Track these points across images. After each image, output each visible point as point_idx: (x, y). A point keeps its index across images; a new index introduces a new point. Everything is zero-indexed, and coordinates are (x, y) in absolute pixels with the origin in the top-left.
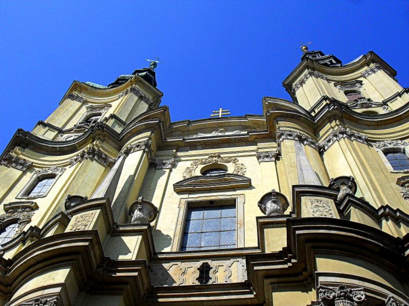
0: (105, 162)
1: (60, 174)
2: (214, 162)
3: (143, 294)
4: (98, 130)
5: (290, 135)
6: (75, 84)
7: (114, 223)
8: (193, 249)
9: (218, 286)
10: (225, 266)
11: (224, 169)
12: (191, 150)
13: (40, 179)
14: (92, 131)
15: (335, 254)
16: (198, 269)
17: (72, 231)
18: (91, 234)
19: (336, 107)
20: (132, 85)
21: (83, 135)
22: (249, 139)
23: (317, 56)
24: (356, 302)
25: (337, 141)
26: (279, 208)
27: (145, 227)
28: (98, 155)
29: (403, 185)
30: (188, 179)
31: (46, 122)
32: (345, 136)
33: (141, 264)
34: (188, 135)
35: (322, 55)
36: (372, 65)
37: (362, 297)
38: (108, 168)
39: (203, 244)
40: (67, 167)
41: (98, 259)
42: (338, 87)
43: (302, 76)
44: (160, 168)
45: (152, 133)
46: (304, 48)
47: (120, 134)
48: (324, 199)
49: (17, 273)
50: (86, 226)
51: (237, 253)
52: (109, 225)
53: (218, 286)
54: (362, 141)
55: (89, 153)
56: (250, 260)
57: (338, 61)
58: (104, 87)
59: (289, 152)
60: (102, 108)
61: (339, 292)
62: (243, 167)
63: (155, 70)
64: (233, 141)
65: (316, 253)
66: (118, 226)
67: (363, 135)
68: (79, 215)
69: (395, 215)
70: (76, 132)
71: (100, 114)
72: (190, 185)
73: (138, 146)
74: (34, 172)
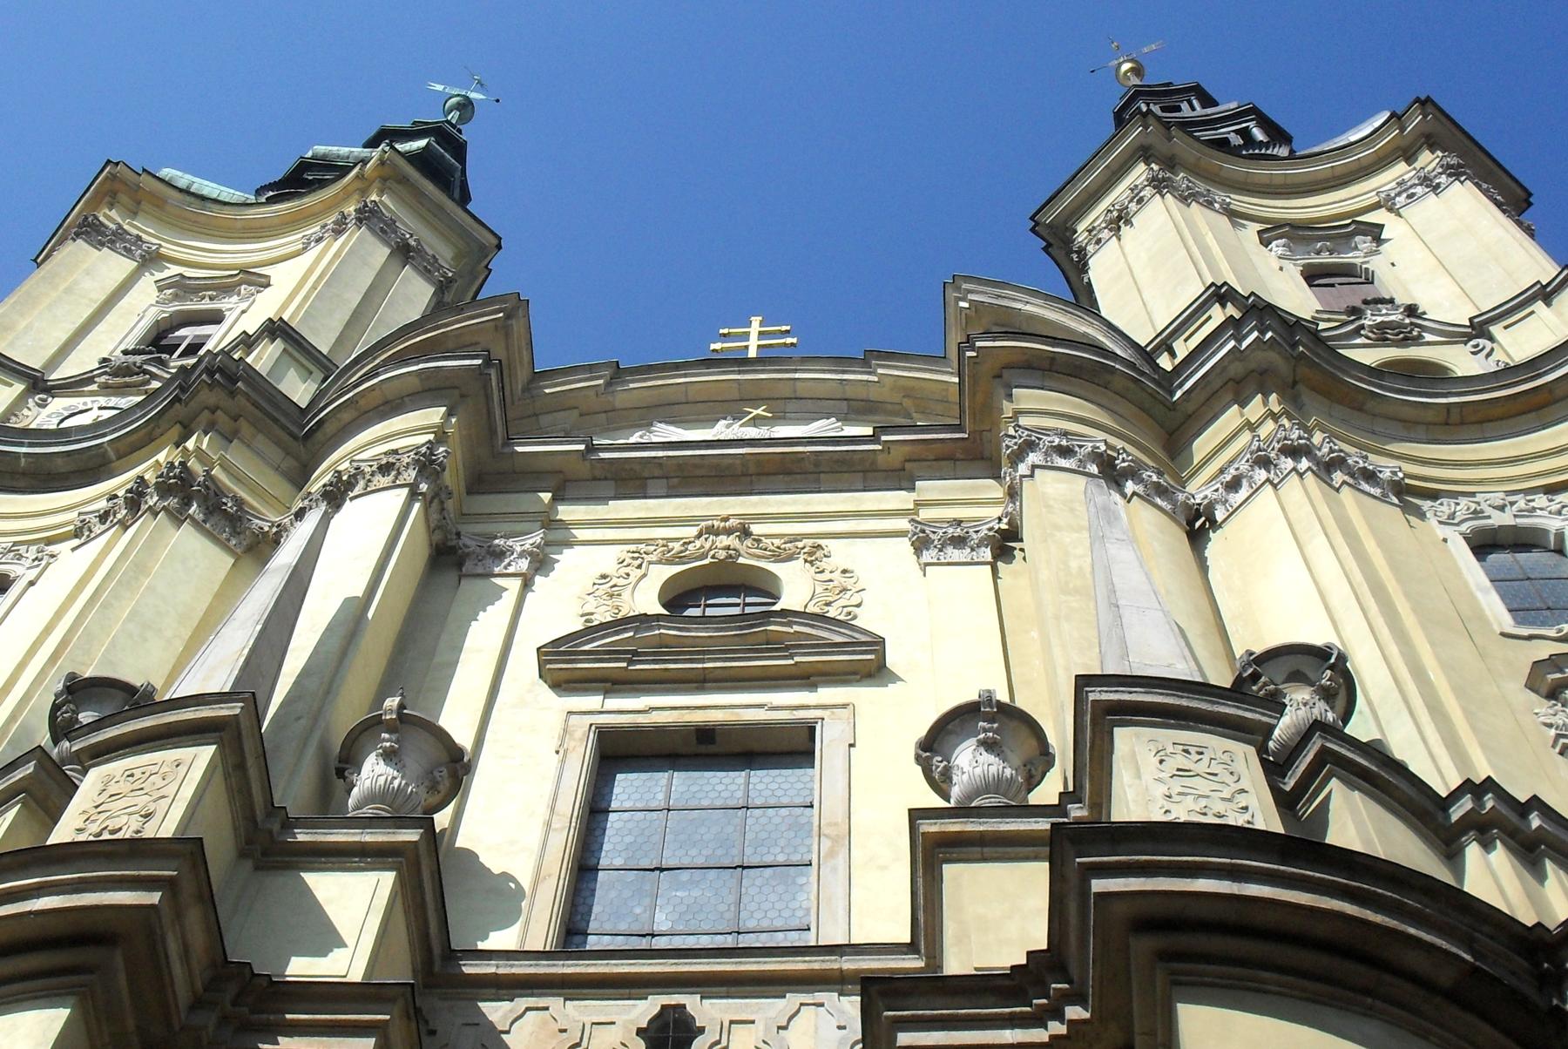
1: (32, 574)
2: (722, 555)
5: (1066, 452)
6: (113, 177)
7: (273, 810)
10: (760, 1026)
11: (762, 586)
14: (183, 389)
16: (640, 1032)
17: (82, 838)
19: (1269, 334)
20: (364, 192)
22: (881, 458)
23: (1185, 106)
25: (1268, 488)
27: (411, 835)
29: (1553, 694)
30: (603, 626)
32: (1304, 464)
33: (392, 1000)
35: (1208, 101)
36: (1428, 160)
39: (662, 922)
40: (63, 548)
42: (1278, 247)
43: (1120, 192)
44: (480, 570)
45: (449, 414)
46: (1126, 66)
47: (303, 412)
48: (1215, 743)
50: (148, 816)
51: (816, 966)
54: (1377, 491)
55: (164, 489)
57: (1278, 135)
59: (1057, 527)
62: (849, 583)
63: (468, 133)
66: (289, 824)
68: (117, 767)
70: (107, 389)
71: (216, 318)
73: (385, 469)
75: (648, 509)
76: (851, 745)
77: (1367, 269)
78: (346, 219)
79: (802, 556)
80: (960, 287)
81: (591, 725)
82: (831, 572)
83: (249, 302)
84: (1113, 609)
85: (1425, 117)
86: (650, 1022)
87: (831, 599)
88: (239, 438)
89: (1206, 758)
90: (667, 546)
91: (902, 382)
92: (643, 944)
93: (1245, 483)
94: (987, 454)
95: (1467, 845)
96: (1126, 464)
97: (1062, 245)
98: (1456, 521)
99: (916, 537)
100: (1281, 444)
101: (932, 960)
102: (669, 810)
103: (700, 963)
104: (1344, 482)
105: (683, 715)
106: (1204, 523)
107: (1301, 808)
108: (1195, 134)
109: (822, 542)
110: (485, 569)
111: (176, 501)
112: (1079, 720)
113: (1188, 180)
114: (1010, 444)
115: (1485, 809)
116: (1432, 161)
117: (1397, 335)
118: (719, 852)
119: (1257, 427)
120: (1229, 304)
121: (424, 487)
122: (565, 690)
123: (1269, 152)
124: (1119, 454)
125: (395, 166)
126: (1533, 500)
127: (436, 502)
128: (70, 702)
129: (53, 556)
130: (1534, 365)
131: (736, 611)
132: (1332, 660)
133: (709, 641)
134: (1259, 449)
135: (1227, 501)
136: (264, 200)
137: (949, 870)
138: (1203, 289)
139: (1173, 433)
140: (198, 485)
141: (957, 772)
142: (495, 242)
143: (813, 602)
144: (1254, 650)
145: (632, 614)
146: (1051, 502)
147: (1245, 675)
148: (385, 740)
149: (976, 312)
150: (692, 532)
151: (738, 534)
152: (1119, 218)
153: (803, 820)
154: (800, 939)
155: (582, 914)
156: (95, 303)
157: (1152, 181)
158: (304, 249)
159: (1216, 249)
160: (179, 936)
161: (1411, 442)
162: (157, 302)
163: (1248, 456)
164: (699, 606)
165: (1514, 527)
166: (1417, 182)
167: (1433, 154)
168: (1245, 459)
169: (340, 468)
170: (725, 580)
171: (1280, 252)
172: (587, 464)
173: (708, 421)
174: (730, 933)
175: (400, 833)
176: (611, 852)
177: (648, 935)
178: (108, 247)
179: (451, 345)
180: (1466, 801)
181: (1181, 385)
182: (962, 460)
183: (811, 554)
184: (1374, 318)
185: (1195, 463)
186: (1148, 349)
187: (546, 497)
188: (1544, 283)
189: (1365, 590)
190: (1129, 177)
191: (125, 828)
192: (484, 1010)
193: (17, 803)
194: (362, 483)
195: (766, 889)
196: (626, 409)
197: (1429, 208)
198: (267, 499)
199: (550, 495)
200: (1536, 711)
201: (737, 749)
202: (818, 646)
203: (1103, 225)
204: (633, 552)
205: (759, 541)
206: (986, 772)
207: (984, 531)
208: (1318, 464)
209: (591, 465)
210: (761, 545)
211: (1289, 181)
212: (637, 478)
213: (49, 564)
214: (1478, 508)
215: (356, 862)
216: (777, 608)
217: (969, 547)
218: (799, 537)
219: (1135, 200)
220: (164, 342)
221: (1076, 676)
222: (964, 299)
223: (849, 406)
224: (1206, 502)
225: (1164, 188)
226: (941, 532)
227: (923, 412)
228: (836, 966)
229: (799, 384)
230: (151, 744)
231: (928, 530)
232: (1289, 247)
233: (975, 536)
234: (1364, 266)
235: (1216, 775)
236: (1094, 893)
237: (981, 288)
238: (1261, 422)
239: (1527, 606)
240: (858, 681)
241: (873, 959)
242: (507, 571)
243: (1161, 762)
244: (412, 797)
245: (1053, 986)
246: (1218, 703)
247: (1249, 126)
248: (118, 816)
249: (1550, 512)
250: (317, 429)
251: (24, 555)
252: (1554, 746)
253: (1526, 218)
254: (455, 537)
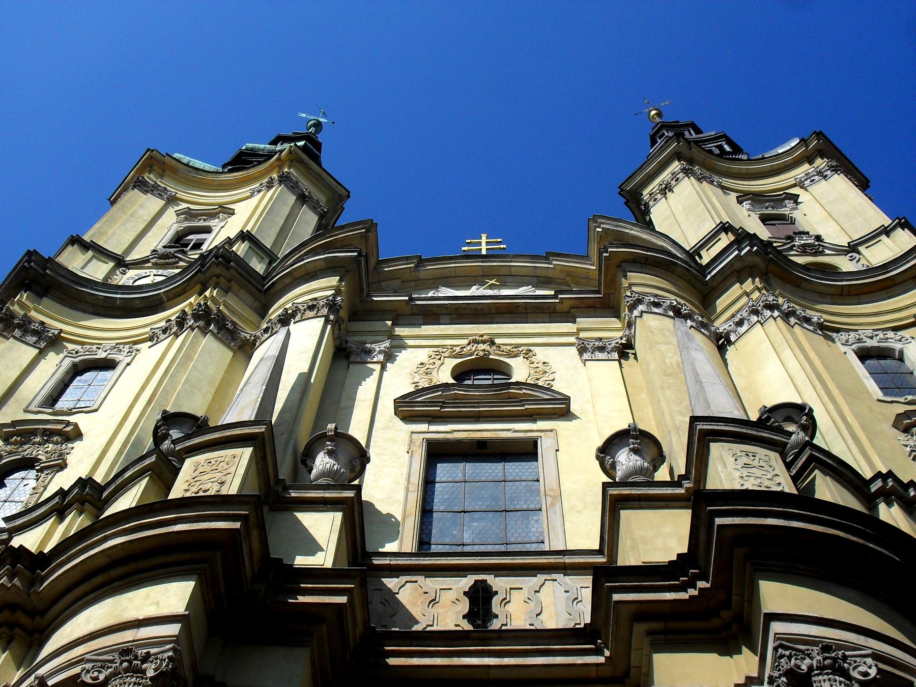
0: (233, 340)
1: (128, 359)
2: (481, 354)
4: (217, 265)
5: (657, 305)
6: (151, 157)
7: (278, 481)
8: (446, 549)
10: (525, 591)
11: (503, 370)
13: (78, 370)
14: (202, 266)
16: (465, 593)
17: (188, 495)
19: (755, 248)
20: (281, 167)
22: (558, 307)
24: (858, 681)
25: (759, 325)
26: (646, 464)
27: (350, 494)
29: (906, 430)
30: (424, 389)
31: (87, 238)
32: (776, 313)
34: (419, 289)
35: (698, 131)
36: (820, 163)
37: (870, 671)
38: (241, 357)
39: (467, 538)
40: (144, 346)
42: (746, 205)
43: (665, 175)
44: (359, 360)
45: (341, 280)
46: (653, 112)
48: (761, 452)
49: (61, 586)
50: (222, 483)
51: (552, 561)
53: (513, 634)
54: (811, 328)
55: (196, 317)
57: (737, 149)
58: (213, 168)
59: (658, 343)
60: (212, 215)
61: (819, 658)
62: (547, 369)
63: (320, 138)
66: (286, 488)
67: (815, 317)
68: (201, 458)
69: (905, 494)
70: (156, 266)
71: (208, 230)
73: (311, 308)
74: (65, 353)
75: (441, 330)
77: (791, 217)
78: (273, 181)
79: (522, 355)
80: (597, 221)
81: (423, 439)
83: (225, 223)
84: (699, 384)
85: (819, 141)
86: (470, 588)
87: (539, 377)
89: (757, 459)
90: (453, 349)
91: (564, 268)
92: (459, 549)
95: (880, 503)
96: (687, 312)
98: (849, 344)
99: (580, 346)
100: (764, 303)
101: (610, 559)
103: (493, 559)
104: (796, 323)
105: (470, 434)
106: (724, 342)
107: (799, 484)
108: (702, 146)
109: (531, 348)
110: (361, 359)
111: (203, 323)
113: (701, 170)
114: (629, 300)
115: (888, 486)
116: (822, 164)
117: (812, 250)
118: (493, 503)
119: (750, 294)
121: (332, 317)
122: (408, 421)
123: (737, 157)
126: (886, 334)
127: (337, 324)
128: (165, 425)
129: (138, 350)
130: (885, 267)
131: (490, 382)
132: (806, 411)
133: (480, 397)
134: (753, 305)
136: (227, 171)
137: (624, 513)
138: (715, 226)
140: (214, 315)
143: (530, 378)
145: (438, 383)
146: (653, 330)
147: (763, 418)
148: (328, 445)
149: (605, 234)
151: (489, 343)
152: (666, 188)
153: (534, 488)
154: (538, 547)
156: (146, 221)
159: (718, 205)
161: (826, 304)
162: (177, 222)
163: (747, 308)
164: (470, 379)
165: (878, 347)
166: (815, 174)
167: (822, 160)
168: (745, 311)
170: (481, 367)
171: (748, 207)
173: (467, 286)
174: (503, 544)
175: (344, 493)
176: (438, 504)
178: (151, 193)
180: (879, 482)
181: (710, 273)
182: (599, 308)
183: (526, 354)
184: (800, 241)
186: (691, 252)
187: (389, 323)
188: (886, 226)
189: (813, 376)
190: (670, 168)
191: (211, 489)
193: (147, 476)
194: (299, 315)
195: (520, 523)
196: (425, 279)
197: (821, 188)
198: (247, 322)
199: (391, 322)
200: (899, 438)
202: (536, 400)
203: (658, 192)
204: (436, 352)
206: (635, 465)
210: (500, 349)
212: (433, 315)
213: (136, 354)
214: (860, 337)
215: (321, 507)
216: (510, 381)
217: (607, 352)
218: (519, 346)
219: (674, 179)
222: (599, 227)
223: (538, 280)
225: (689, 173)
226: (592, 344)
227: (577, 284)
229: (513, 268)
232: (752, 205)
233: (609, 346)
234: (790, 215)
236: (717, 525)
238: (752, 292)
239: (887, 386)
240: (556, 418)
241: (581, 558)
242: (373, 361)
243: (736, 460)
245: (691, 571)
247: (722, 144)
248: (206, 483)
249: (896, 340)
251: (122, 350)
252: (909, 456)
253: (867, 191)
254: (345, 343)
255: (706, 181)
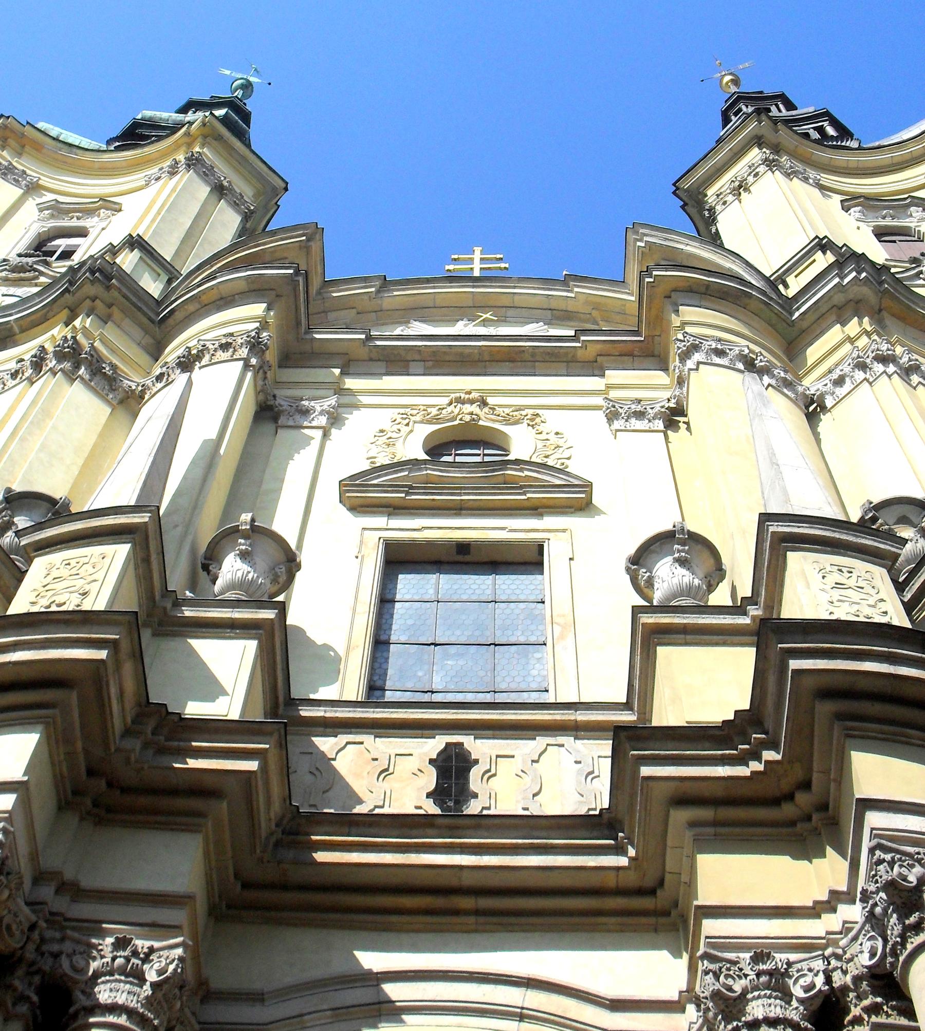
0: (112, 390)
2: (467, 418)
3: (264, 835)
5: (720, 353)
7: (166, 592)
9: (513, 821)
10: (518, 759)
12: (389, 373)
14: (71, 283)
15: (907, 743)
16: (431, 761)
18: (116, 623)
19: (864, 275)
20: (190, 145)
21: (38, 294)
23: (773, 108)
27: (269, 614)
28: (90, 365)
30: (383, 467)
32: (891, 368)
33: (270, 734)
35: (790, 106)
38: (121, 414)
41: (128, 706)
42: (855, 211)
43: (739, 169)
44: (291, 423)
45: (269, 309)
46: (727, 78)
47: (158, 303)
48: (860, 566)
50: (85, 594)
51: (558, 717)
52: (152, 598)
55: (60, 356)
56: (627, 746)
57: (844, 132)
58: (94, 145)
60: (90, 212)
62: (561, 442)
63: (250, 105)
64: (527, 356)
65: (849, 736)
66: (178, 603)
71: (82, 233)
72: (394, 487)
73: (225, 347)
76: (571, 559)
79: (526, 422)
81: (380, 538)
82: (547, 434)
86: (439, 754)
88: (112, 321)
89: (854, 575)
91: (591, 298)
92: (426, 698)
93: (847, 379)
94: (656, 353)
97: (696, 205)
100: (874, 353)
102: (438, 602)
103: (473, 713)
106: (816, 408)
112: (759, 546)
118: (477, 633)
119: (855, 341)
120: (828, 251)
121: (254, 361)
122: (359, 512)
123: (843, 144)
124: (757, 356)
125: (213, 128)
131: (478, 459)
134: (859, 357)
135: (834, 393)
139: (791, 342)
140: (86, 354)
141: (658, 581)
142: (283, 185)
144: (872, 500)
147: (867, 518)
148: (241, 544)
150: (444, 401)
152: (740, 187)
153: (537, 612)
155: (380, 675)
157: (765, 162)
158: (147, 185)
160: (117, 682)
163: (850, 360)
164: (450, 455)
168: (848, 363)
169: (190, 345)
171: (857, 216)
172: (367, 349)
176: (398, 633)
177: (428, 691)
179: (268, 258)
181: (798, 309)
182: (640, 356)
185: (808, 366)
186: (772, 279)
187: (337, 371)
191: (68, 603)
192: (316, 743)
199: (339, 370)
201: (486, 559)
202: (544, 486)
203: (729, 191)
205: (493, 409)
207: (658, 408)
208: (901, 369)
209: (369, 349)
211: (861, 166)
212: (402, 361)
219: (752, 174)
220: (44, 249)
221: (760, 514)
222: (641, 240)
224: (818, 393)
225: (774, 166)
228: (573, 718)
229: (516, 297)
230: (82, 542)
231: (617, 406)
232: (863, 213)
233: (650, 411)
235: (862, 588)
237: (653, 233)
238: (858, 337)
243: (824, 577)
244: (262, 586)
246: (860, 537)
250: (168, 317)
255: (798, 178)
